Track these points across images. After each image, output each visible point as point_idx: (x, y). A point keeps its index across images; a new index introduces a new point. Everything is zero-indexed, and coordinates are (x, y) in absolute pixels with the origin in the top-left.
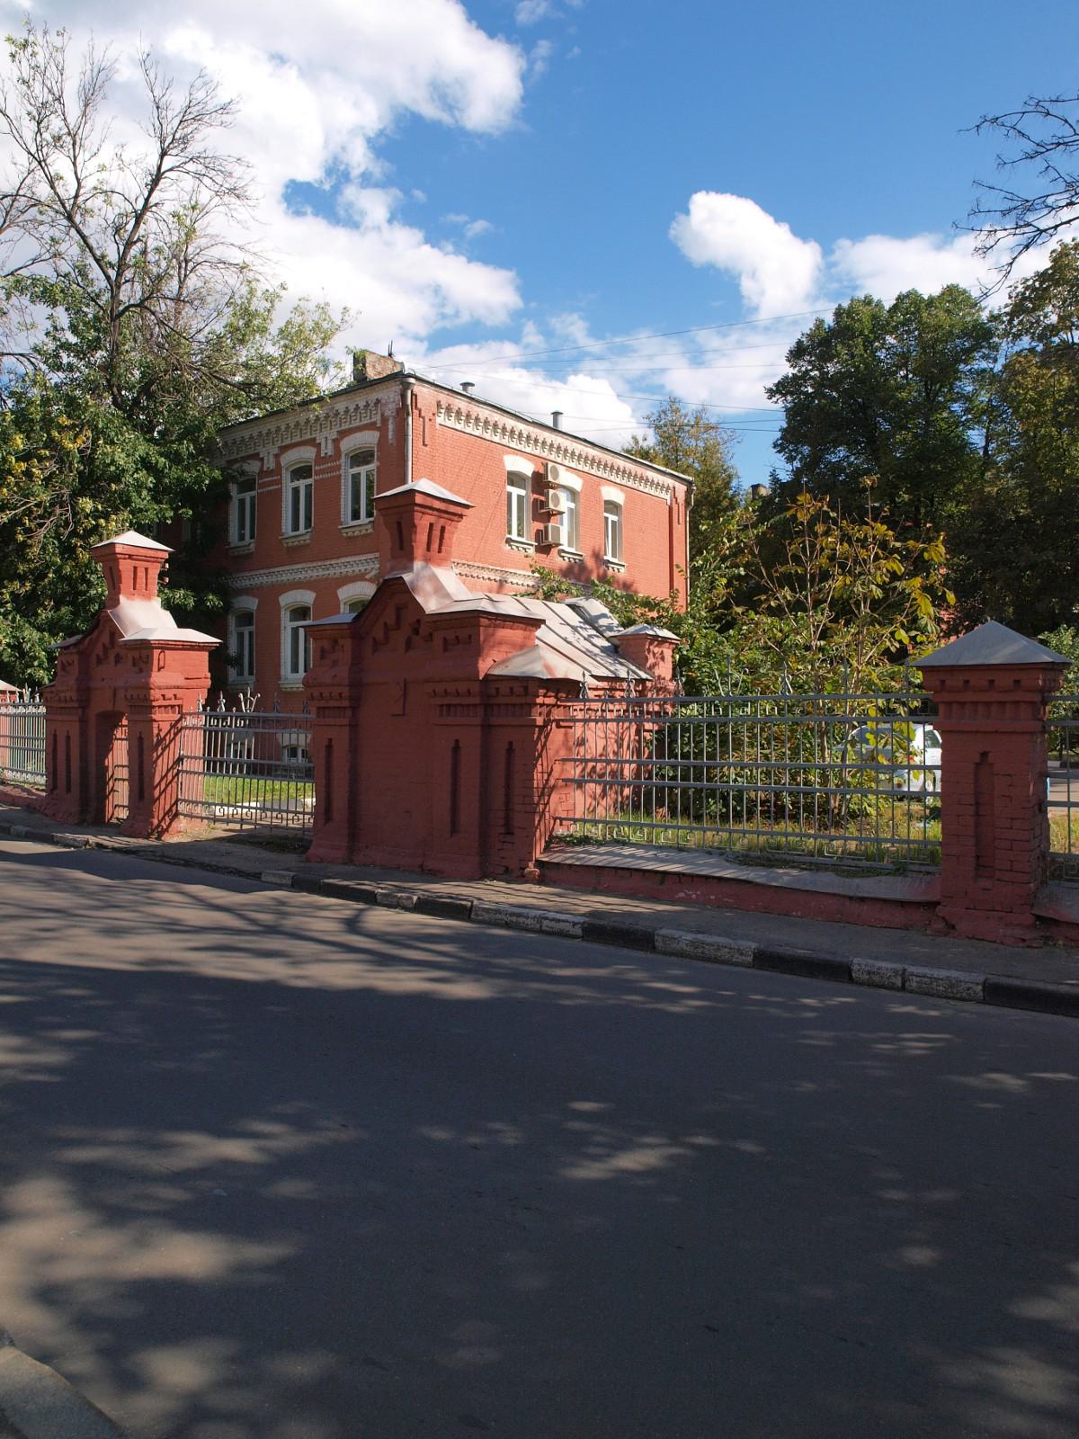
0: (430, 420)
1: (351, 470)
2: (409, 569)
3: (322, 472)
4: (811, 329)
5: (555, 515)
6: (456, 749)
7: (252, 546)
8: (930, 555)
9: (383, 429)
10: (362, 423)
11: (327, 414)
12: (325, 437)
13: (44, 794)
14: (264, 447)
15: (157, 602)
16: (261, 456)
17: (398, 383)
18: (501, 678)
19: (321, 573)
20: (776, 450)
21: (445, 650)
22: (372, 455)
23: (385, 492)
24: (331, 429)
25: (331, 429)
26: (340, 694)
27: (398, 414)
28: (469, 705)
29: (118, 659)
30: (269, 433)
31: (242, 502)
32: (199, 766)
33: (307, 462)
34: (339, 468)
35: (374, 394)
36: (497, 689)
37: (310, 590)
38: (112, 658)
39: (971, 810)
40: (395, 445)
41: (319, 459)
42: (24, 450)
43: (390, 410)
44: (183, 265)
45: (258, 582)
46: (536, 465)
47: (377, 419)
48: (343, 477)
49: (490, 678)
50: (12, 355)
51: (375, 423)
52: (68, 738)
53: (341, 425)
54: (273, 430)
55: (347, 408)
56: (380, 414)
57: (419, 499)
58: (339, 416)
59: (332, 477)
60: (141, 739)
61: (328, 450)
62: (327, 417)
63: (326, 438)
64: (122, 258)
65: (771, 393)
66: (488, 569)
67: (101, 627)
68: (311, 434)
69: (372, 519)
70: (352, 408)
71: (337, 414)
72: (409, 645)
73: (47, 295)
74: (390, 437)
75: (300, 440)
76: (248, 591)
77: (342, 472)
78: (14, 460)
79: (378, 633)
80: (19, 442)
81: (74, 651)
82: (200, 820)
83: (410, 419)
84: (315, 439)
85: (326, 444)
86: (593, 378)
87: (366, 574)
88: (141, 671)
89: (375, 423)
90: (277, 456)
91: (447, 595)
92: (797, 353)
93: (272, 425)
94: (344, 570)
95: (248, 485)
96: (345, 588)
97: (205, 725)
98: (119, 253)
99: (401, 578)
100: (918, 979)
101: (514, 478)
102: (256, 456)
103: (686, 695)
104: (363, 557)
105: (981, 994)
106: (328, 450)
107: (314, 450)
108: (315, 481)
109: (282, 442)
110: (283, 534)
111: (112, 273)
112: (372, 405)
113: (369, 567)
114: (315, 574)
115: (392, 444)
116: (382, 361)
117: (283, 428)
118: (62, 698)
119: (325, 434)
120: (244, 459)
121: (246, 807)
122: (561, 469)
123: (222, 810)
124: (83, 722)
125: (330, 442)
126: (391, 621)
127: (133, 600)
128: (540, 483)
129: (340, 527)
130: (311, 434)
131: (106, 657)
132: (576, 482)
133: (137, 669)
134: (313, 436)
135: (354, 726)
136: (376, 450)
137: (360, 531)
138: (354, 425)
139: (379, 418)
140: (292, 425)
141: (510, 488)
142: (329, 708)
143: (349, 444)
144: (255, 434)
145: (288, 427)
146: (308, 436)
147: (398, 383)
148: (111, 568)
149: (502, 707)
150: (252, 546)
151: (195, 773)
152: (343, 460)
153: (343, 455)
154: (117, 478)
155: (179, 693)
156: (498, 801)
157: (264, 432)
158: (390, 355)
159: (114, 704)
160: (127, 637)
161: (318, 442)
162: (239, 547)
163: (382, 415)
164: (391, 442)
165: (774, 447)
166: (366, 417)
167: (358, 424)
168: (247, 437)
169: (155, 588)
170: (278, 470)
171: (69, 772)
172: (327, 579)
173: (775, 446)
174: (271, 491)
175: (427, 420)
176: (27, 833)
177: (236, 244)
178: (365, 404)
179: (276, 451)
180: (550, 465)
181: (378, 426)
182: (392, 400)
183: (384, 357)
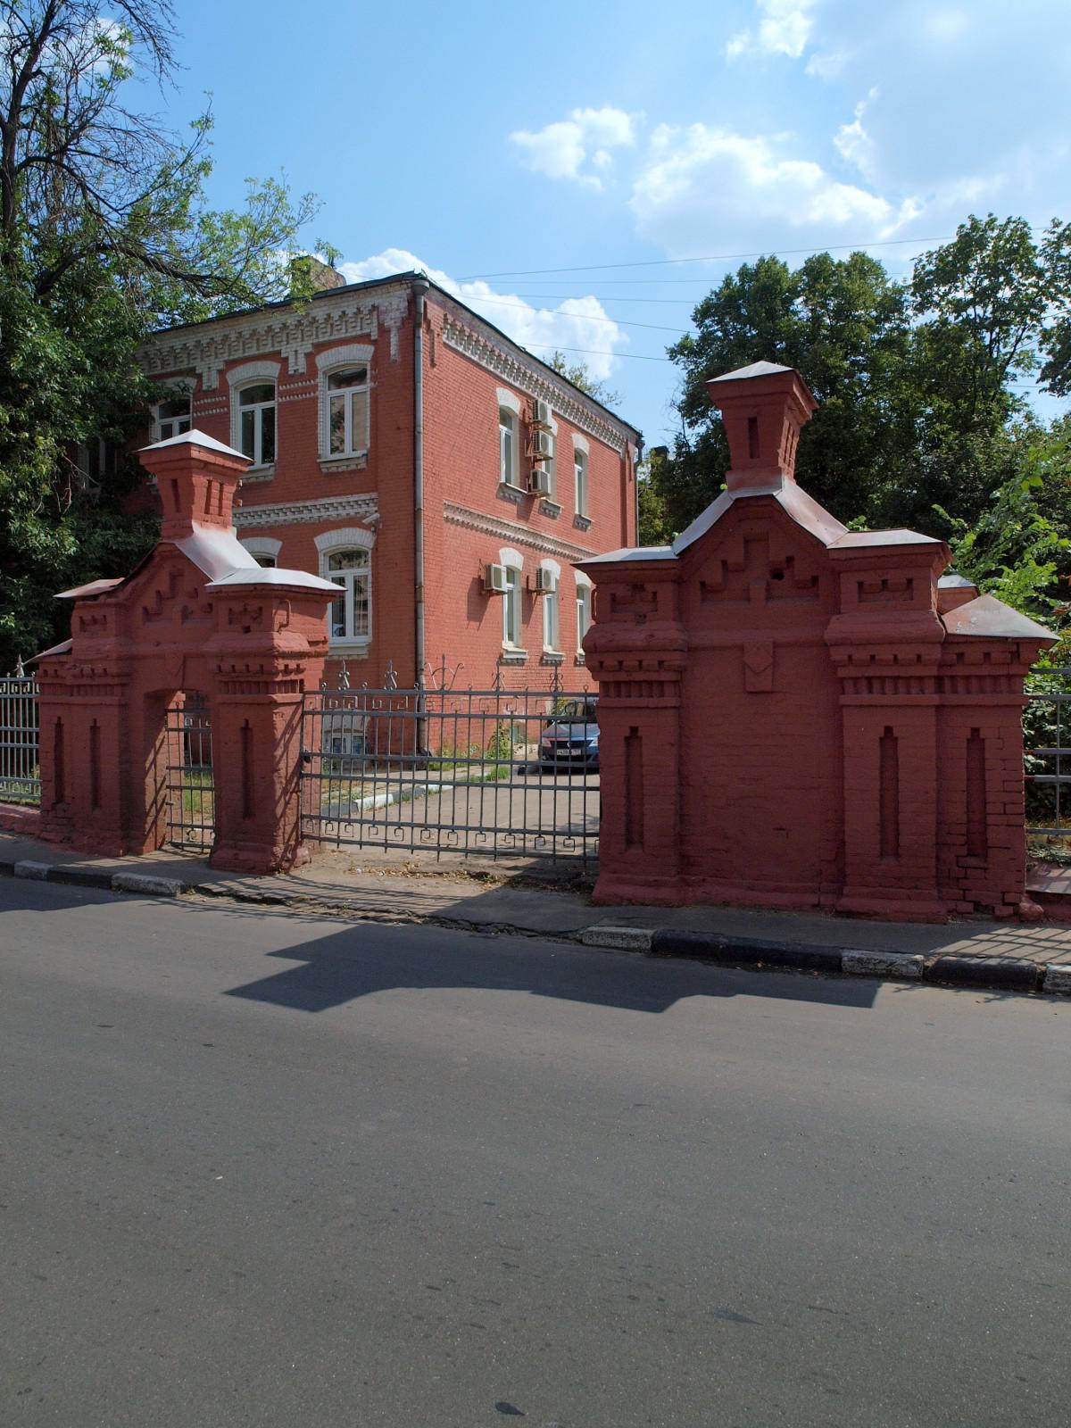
0: (438, 335)
1: (329, 392)
3: (289, 393)
4: (1031, 238)
9: (380, 344)
11: (299, 321)
13: (36, 812)
14: (202, 360)
17: (405, 286)
18: (973, 640)
19: (290, 517)
22: (364, 372)
23: (715, 377)
24: (303, 340)
25: (303, 340)
33: (269, 381)
34: (315, 388)
35: (369, 299)
37: (273, 537)
40: (399, 360)
41: (285, 376)
43: (393, 319)
49: (951, 639)
51: (369, 335)
53: (317, 337)
56: (375, 324)
57: (195, 454)
58: (331, 321)
59: (303, 400)
63: (296, 351)
65: (673, 354)
66: (487, 518)
68: (273, 346)
70: (336, 315)
74: (393, 352)
75: (257, 353)
79: (149, 600)
85: (296, 358)
89: (369, 335)
92: (702, 314)
93: (217, 333)
94: (324, 514)
96: (326, 535)
99: (772, 497)
101: (505, 417)
104: (352, 498)
106: (298, 365)
108: (279, 404)
110: (319, 457)
114: (282, 517)
117: (233, 336)
119: (294, 345)
129: (319, 461)
138: (337, 337)
140: (246, 334)
144: (191, 344)
146: (269, 349)
148: (175, 482)
149: (82, 688)
157: (204, 342)
161: (197, 372)
164: (393, 358)
167: (343, 336)
169: (228, 512)
170: (224, 389)
172: (298, 524)
174: (213, 415)
176: (50, 872)
177: (128, 112)
178: (355, 310)
179: (309, 349)
181: (372, 338)
182: (395, 307)
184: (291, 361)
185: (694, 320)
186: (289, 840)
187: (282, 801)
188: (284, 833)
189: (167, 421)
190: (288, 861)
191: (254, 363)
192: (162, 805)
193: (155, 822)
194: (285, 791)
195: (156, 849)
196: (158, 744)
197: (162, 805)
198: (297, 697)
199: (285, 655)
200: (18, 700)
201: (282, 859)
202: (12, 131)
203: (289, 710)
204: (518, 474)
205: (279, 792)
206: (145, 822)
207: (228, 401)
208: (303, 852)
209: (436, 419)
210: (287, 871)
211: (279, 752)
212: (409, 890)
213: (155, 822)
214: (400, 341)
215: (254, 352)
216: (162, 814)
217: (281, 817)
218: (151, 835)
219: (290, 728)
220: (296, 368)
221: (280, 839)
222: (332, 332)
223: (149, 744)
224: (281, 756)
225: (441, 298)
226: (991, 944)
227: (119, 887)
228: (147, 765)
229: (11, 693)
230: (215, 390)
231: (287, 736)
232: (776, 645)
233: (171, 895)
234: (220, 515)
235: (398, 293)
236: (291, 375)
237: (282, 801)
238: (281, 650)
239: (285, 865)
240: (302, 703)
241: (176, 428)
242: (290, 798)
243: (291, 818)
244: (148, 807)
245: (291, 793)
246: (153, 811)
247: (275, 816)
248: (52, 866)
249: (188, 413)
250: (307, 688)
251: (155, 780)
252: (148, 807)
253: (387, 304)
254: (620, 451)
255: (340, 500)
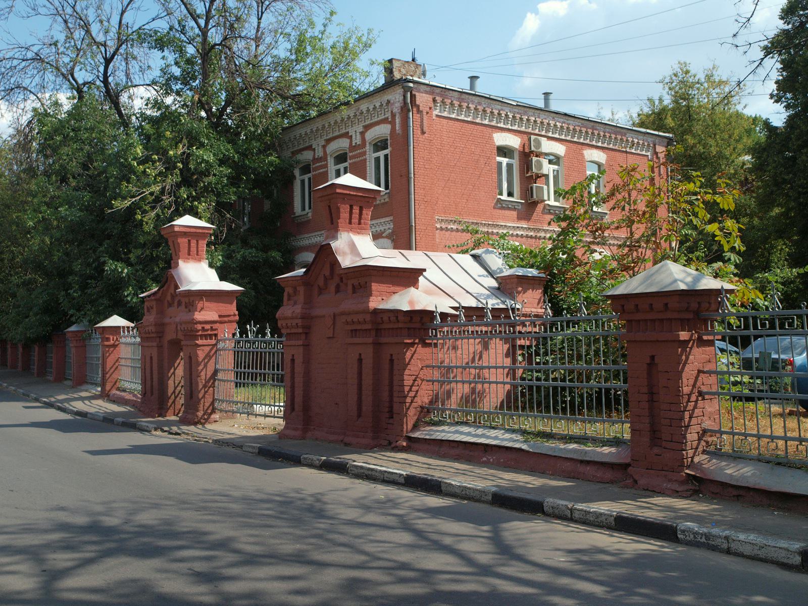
0: (427, 113)
2: (335, 238)
5: (541, 177)
6: (360, 360)
7: (310, 215)
8: (307, 248)
9: (393, 123)
10: (379, 119)
12: (355, 131)
14: (315, 140)
15: (204, 265)
16: (313, 147)
20: (773, 101)
21: (354, 292)
24: (358, 124)
26: (297, 324)
27: (402, 110)
28: (389, 329)
29: (179, 304)
30: (318, 130)
31: (303, 182)
32: (231, 376)
33: (344, 150)
34: (364, 153)
36: (382, 318)
38: (176, 304)
39: (645, 397)
40: (400, 133)
42: (142, 156)
43: (396, 107)
44: (260, 5)
45: (314, 242)
46: (522, 138)
47: (388, 115)
48: (368, 160)
50: (142, 85)
51: (388, 118)
52: (151, 358)
54: (320, 127)
55: (368, 108)
60: (190, 357)
61: (357, 140)
62: (355, 116)
64: (208, 12)
66: (482, 224)
67: (168, 283)
68: (346, 129)
69: (388, 191)
70: (371, 108)
71: (362, 113)
72: (338, 290)
73: (161, 43)
74: (397, 128)
76: (307, 248)
77: (367, 156)
78: (136, 164)
79: (321, 282)
80: (139, 151)
81: (153, 298)
82: (649, 489)
83: (411, 113)
84: (348, 133)
85: (356, 136)
86: (783, 10)
87: (383, 233)
88: (190, 311)
89: (388, 118)
90: (324, 147)
91: (358, 254)
95: (306, 169)
97: (235, 347)
98: (206, 8)
100: (579, 512)
101: (504, 151)
102: (310, 148)
103: (493, 319)
104: (383, 220)
105: (613, 523)
106: (357, 140)
107: (348, 141)
108: (350, 164)
109: (327, 136)
111: (202, 22)
112: (385, 105)
113: (386, 228)
115: (399, 134)
116: (406, 66)
117: (327, 126)
118: (147, 331)
119: (355, 128)
120: (300, 151)
121: (277, 406)
122: (544, 141)
123: (270, 409)
124: (160, 347)
125: (358, 134)
126: (327, 273)
127: (187, 262)
128: (526, 156)
130: (346, 129)
131: (173, 303)
132: (559, 149)
133: (187, 310)
134: (347, 130)
135: (307, 346)
136: (389, 138)
137: (380, 200)
139: (390, 114)
140: (332, 123)
141: (499, 159)
142: (292, 333)
143: (372, 134)
145: (330, 125)
146: (344, 131)
147: (401, 87)
150: (310, 215)
151: (228, 381)
152: (368, 147)
153: (367, 144)
154: (206, 173)
155: (215, 326)
156: (385, 395)
157: (314, 129)
158: (413, 60)
159: (177, 334)
160: (182, 288)
161: (350, 134)
162: (301, 216)
163: (392, 112)
164: (398, 132)
165: (771, 98)
166: (388, 111)
167: (376, 120)
168: (308, 131)
170: (324, 158)
171: (152, 378)
173: (772, 96)
175: (425, 114)
176: (123, 422)
178: (379, 104)
179: (323, 143)
180: (533, 137)
181: (390, 120)
182: (397, 100)
183: (408, 62)
184: (354, 137)
185: (782, 18)
186: (207, 410)
187: (203, 391)
188: (204, 406)
189: (338, 167)
190: (205, 419)
191: (337, 140)
192: (178, 394)
193: (174, 402)
194: (205, 386)
195: (174, 415)
196: (176, 365)
197: (178, 394)
198: (213, 342)
199: (200, 323)
200: (257, 353)
201: (201, 418)
202: (205, 32)
203: (208, 349)
204: (519, 189)
205: (201, 387)
206: (168, 402)
207: (327, 164)
208: (216, 416)
209: (426, 167)
210: (203, 424)
211: (200, 368)
212: (775, 545)
213: (174, 402)
214: (402, 121)
215: (337, 133)
216: (178, 399)
217: (202, 398)
218: (171, 408)
219: (208, 356)
220: (356, 141)
221: (201, 408)
222: (371, 118)
223: (171, 364)
224: (202, 370)
225: (428, 89)
226: (694, 509)
227: (138, 428)
228: (170, 375)
229: (261, 348)
230: (321, 158)
231: (206, 360)
232: (334, 315)
233: (149, 431)
234: (197, 255)
235: (398, 91)
236: (354, 146)
237: (203, 391)
238: (197, 320)
239: (203, 421)
240: (216, 345)
241: (342, 171)
242: (208, 390)
243: (209, 399)
244: (169, 395)
245: (209, 388)
246: (173, 397)
247: (198, 398)
248: (124, 420)
249: (310, 172)
250: (219, 338)
251: (174, 382)
252: (169, 395)
253: (394, 98)
254: (649, 154)
255: (377, 222)
